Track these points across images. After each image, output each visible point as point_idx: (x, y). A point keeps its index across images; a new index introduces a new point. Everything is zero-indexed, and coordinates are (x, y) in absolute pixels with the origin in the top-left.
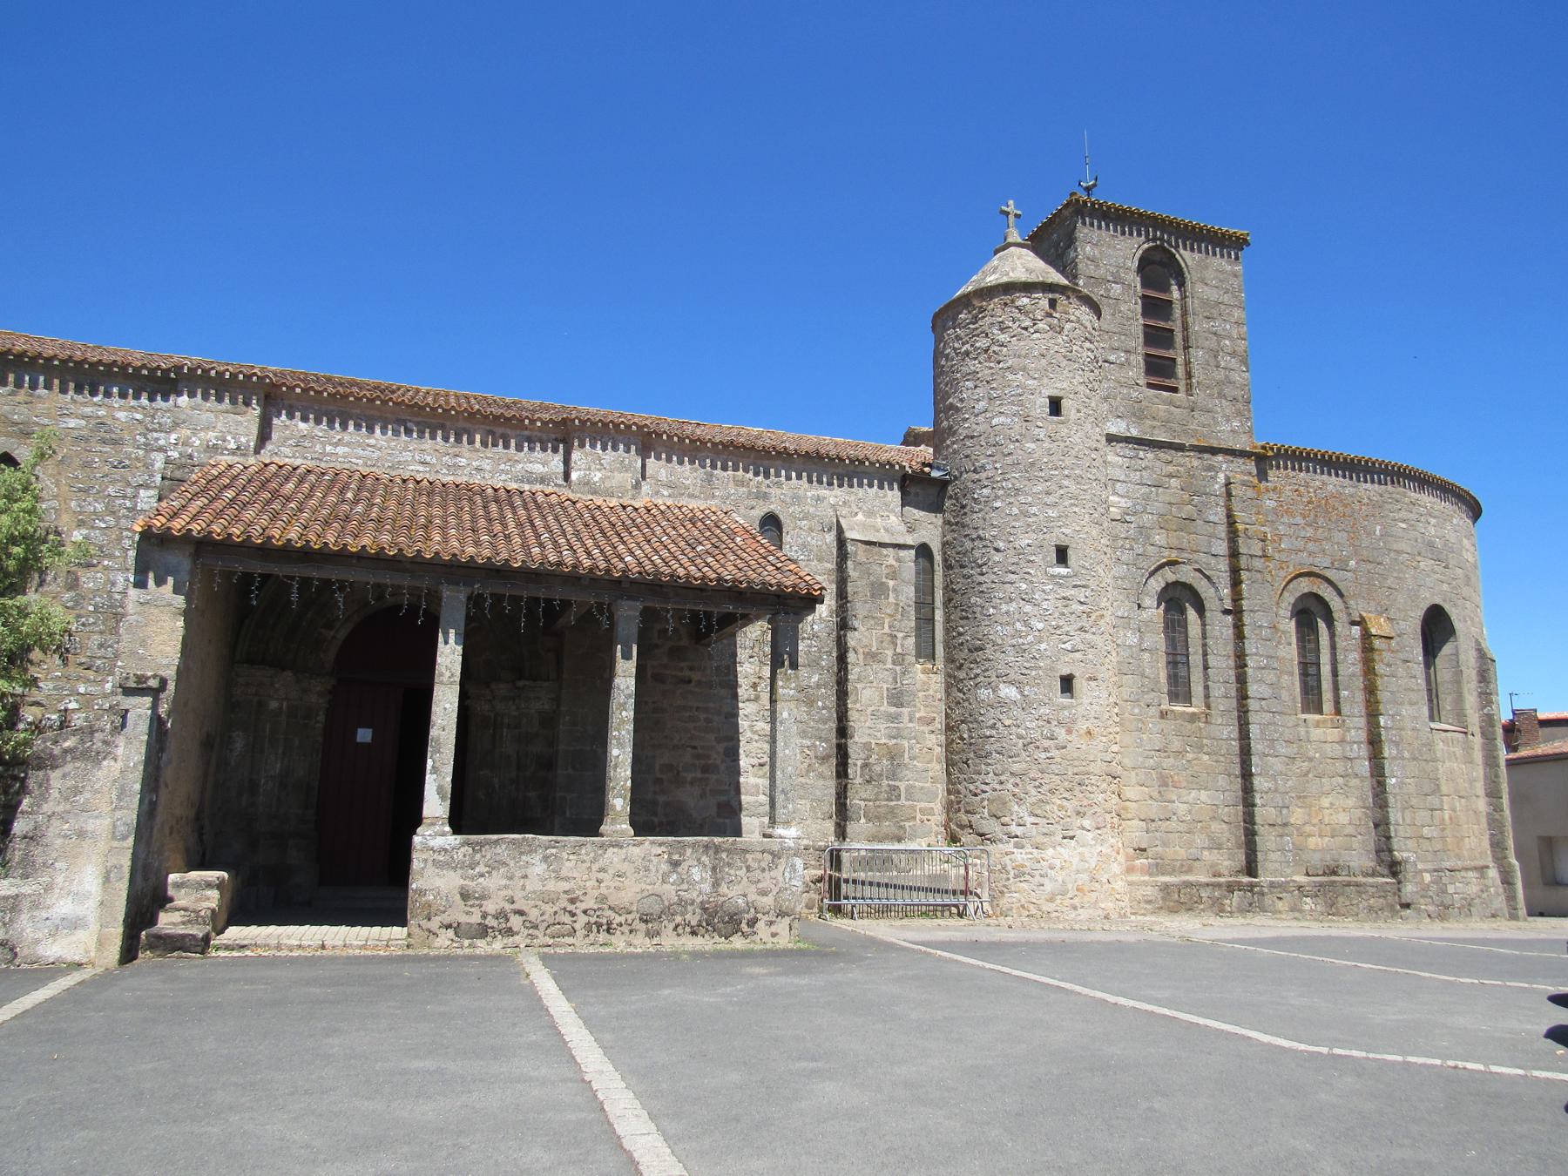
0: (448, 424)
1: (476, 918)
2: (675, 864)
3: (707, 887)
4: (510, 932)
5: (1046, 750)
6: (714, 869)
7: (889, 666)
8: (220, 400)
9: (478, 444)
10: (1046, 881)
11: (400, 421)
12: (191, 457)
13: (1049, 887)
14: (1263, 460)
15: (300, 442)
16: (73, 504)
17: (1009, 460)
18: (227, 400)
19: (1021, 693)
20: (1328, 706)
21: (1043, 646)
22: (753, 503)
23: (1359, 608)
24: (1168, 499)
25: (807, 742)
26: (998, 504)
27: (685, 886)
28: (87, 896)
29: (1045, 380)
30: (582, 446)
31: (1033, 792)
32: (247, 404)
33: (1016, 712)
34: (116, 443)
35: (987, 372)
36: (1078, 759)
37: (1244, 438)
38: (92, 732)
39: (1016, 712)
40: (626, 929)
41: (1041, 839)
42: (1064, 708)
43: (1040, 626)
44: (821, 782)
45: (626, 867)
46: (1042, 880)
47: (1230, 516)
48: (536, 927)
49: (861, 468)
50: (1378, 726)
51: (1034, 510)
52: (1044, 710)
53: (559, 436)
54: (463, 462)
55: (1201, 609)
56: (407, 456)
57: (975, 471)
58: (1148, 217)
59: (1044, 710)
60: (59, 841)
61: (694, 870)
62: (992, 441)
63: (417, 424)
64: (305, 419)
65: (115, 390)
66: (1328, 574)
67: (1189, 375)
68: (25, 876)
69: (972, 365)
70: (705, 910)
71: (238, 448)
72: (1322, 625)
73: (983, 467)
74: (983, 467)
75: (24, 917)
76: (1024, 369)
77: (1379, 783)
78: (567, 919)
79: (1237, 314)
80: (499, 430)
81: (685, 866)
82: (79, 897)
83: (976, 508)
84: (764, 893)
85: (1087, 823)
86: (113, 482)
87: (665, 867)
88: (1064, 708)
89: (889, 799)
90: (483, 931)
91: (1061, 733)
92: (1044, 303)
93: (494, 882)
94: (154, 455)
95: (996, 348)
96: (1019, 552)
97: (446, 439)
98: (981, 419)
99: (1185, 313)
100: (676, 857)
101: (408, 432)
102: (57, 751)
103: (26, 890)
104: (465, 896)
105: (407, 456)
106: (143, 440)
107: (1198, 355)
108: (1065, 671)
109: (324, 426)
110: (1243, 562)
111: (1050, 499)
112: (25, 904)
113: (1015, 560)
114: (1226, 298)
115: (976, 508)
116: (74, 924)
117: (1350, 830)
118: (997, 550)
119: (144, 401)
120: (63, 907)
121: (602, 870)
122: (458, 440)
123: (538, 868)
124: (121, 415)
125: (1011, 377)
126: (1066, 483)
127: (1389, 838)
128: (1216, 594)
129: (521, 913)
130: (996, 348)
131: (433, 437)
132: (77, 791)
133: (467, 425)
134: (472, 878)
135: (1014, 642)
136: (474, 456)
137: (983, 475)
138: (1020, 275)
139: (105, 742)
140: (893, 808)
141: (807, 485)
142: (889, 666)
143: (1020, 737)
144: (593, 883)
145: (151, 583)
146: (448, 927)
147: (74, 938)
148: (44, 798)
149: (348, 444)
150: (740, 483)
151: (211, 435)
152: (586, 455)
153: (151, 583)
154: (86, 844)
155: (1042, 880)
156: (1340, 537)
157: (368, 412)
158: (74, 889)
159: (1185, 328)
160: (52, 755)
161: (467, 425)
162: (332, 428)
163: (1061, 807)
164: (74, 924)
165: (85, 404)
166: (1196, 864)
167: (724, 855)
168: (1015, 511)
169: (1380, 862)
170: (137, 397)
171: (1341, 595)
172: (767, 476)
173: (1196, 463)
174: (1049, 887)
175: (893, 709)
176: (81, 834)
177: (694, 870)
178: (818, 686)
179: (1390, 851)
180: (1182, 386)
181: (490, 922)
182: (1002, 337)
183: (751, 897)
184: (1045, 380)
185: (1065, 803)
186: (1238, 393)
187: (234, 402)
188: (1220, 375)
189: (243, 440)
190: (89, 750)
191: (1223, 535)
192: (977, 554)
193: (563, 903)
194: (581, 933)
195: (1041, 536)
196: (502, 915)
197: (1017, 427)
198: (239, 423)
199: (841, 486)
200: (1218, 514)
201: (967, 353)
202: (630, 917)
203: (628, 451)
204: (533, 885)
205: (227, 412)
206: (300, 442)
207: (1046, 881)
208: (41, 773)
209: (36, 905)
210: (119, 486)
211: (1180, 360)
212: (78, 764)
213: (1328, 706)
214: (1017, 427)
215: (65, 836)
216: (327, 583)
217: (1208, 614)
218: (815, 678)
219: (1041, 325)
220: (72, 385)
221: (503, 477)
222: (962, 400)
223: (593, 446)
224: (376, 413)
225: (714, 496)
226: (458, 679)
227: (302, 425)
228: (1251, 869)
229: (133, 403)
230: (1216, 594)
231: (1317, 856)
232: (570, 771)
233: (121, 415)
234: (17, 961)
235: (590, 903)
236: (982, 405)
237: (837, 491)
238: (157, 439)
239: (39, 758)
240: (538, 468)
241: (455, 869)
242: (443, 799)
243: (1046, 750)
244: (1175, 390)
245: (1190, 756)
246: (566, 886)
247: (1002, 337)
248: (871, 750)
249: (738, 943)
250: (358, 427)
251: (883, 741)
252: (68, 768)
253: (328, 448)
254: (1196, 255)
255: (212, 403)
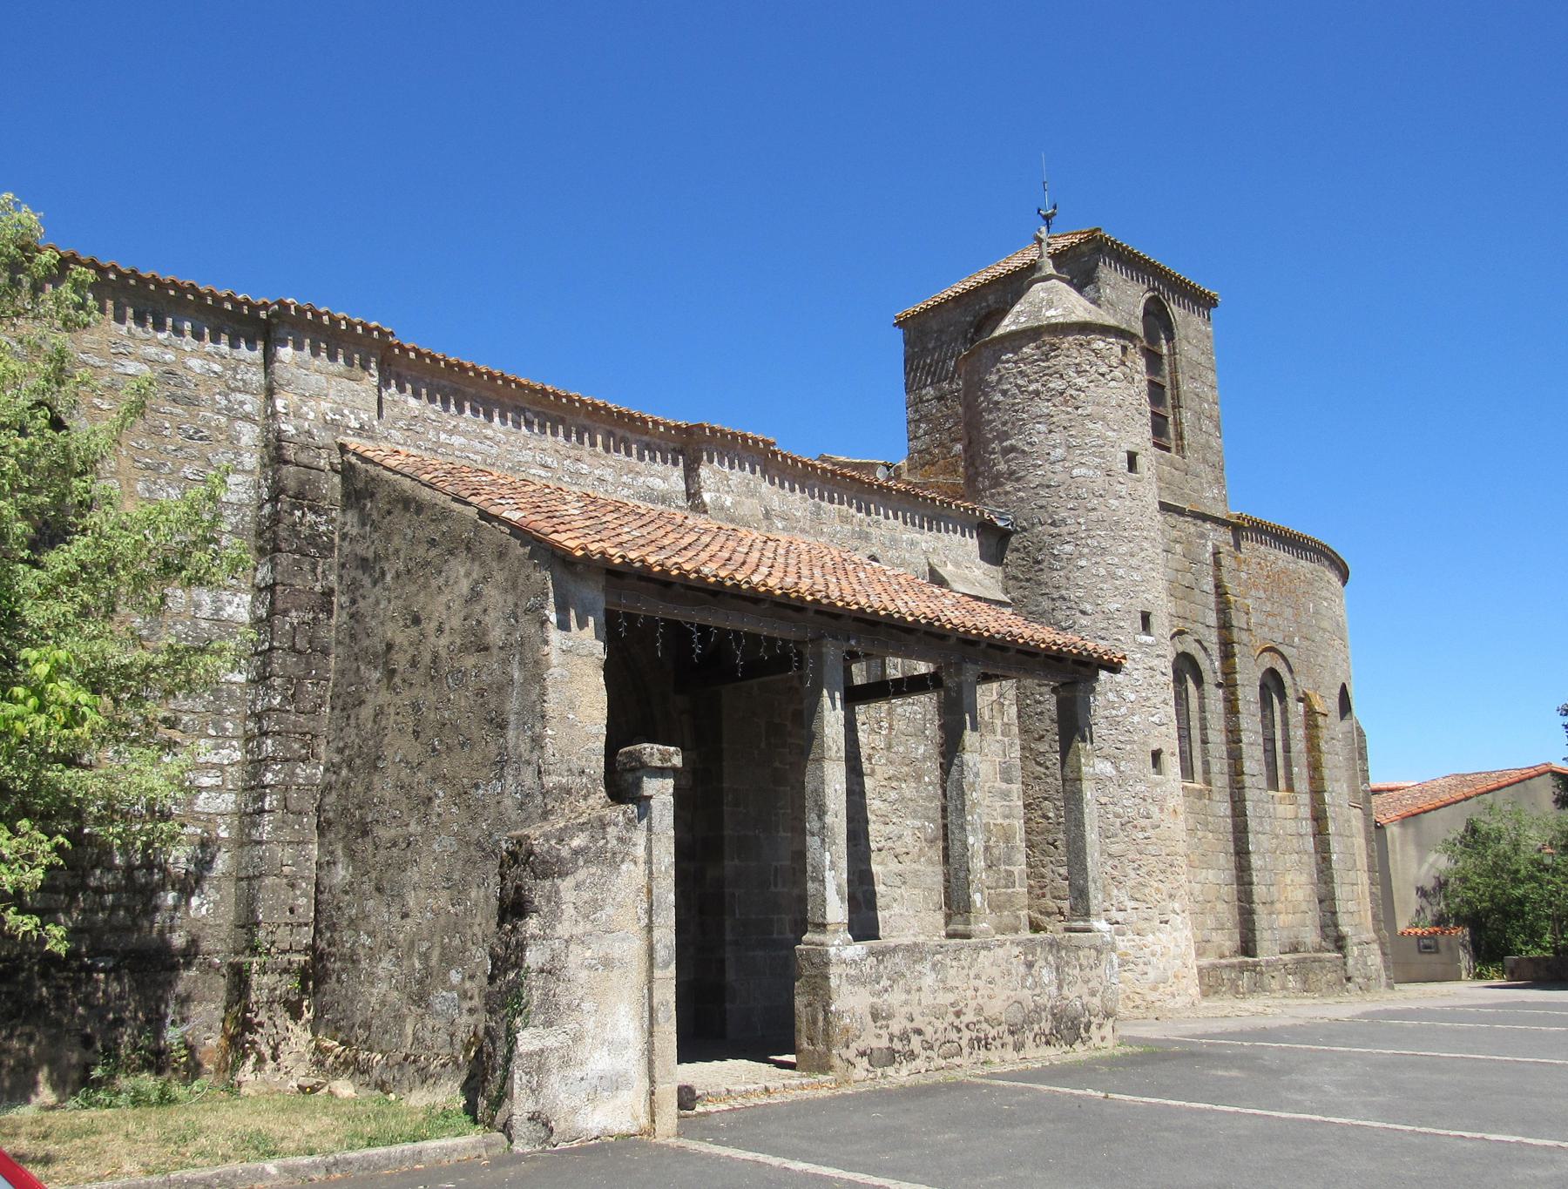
0: (568, 418)
1: (884, 1043)
2: (1030, 965)
3: (1053, 990)
4: (912, 1056)
5: (1143, 829)
6: (1057, 969)
7: (999, 737)
8: (333, 357)
9: (600, 448)
10: (1149, 969)
11: (519, 410)
12: (310, 434)
13: (1152, 975)
14: (1240, 529)
15: (412, 424)
16: (140, 486)
17: (1093, 516)
18: (341, 360)
19: (1117, 768)
20: (1282, 783)
21: (1136, 719)
22: (856, 543)
23: (1304, 685)
24: (1176, 565)
25: (918, 823)
26: (1083, 563)
27: (1038, 991)
28: (625, 1045)
29: (1123, 434)
30: (711, 461)
31: (1132, 874)
32: (365, 367)
33: (1112, 789)
34: (191, 402)
35: (1063, 416)
36: (1169, 839)
37: (1221, 506)
38: (604, 826)
39: (1112, 789)
40: (998, 1043)
41: (1142, 925)
42: (1157, 785)
43: (1133, 697)
44: (930, 869)
45: (995, 972)
46: (1146, 969)
47: (1219, 586)
48: (931, 1048)
49: (947, 512)
50: (1323, 802)
51: (1121, 572)
52: (1140, 787)
53: (678, 446)
54: (585, 468)
55: (1199, 681)
56: (527, 456)
57: (1053, 524)
58: (1152, 264)
59: (1140, 787)
60: (584, 974)
61: (1044, 971)
62: (1073, 493)
63: (537, 415)
64: (417, 395)
65: (187, 326)
66: (1281, 648)
67: (1180, 436)
68: (549, 1024)
69: (1044, 407)
70: (1054, 1015)
71: (362, 428)
72: (1276, 701)
73: (1064, 520)
74: (1064, 520)
75: (554, 1079)
76: (1103, 419)
77: (1324, 859)
78: (954, 1035)
79: (1211, 376)
80: (620, 432)
81: (1036, 967)
82: (615, 1047)
83: (1057, 565)
84: (1093, 994)
85: (1177, 906)
86: (190, 459)
87: (1022, 969)
88: (1157, 785)
89: (1007, 887)
90: (891, 1057)
91: (1154, 810)
92: (1117, 350)
93: (895, 998)
94: (239, 425)
95: (1074, 392)
96: (1108, 616)
97: (567, 437)
98: (1058, 467)
99: (1174, 371)
100: (1030, 958)
101: (529, 424)
102: (565, 852)
103: (551, 1042)
104: (875, 1016)
105: (527, 456)
106: (224, 402)
107: (1187, 416)
108: (1155, 747)
109: (438, 406)
110: (1236, 635)
111: (1134, 562)
112: (554, 1061)
113: (1104, 625)
114: (1202, 359)
115: (1057, 565)
116: (614, 1083)
117: (1304, 907)
118: (1083, 613)
119: (224, 347)
120: (599, 1062)
121: (977, 977)
122: (580, 440)
123: (929, 980)
124: (195, 363)
125: (1091, 426)
126: (1146, 545)
127: (1334, 913)
128: (1211, 666)
129: (919, 1032)
130: (1074, 392)
131: (555, 433)
132: (596, 905)
133: (587, 422)
134: (879, 994)
135: (1107, 713)
136: (595, 462)
137: (1064, 530)
138: (1054, 315)
139: (620, 840)
140: (1010, 896)
141: (902, 526)
142: (999, 737)
143: (1117, 816)
144: (970, 993)
145: (573, 624)
146: (863, 1054)
147: (618, 1102)
148: (555, 915)
149: (464, 434)
150: (845, 519)
151: (325, 406)
152: (715, 473)
153: (573, 624)
154: (615, 974)
155: (1146, 969)
156: (1288, 612)
157: (486, 394)
158: (608, 1036)
159: (1175, 385)
160: (559, 859)
161: (587, 422)
162: (446, 409)
163: (1157, 889)
164: (614, 1083)
165: (147, 342)
166: (1208, 946)
167: (1063, 953)
168: (1103, 572)
169: (1325, 937)
170: (215, 340)
171: (1291, 671)
172: (868, 513)
173: (1193, 529)
174: (1152, 975)
175: (1004, 786)
176: (607, 963)
177: (1044, 971)
178: (925, 759)
179: (1336, 926)
180: (1173, 445)
181: (897, 1045)
182: (1080, 381)
183: (1086, 999)
184: (1123, 434)
185: (1161, 885)
186: (1215, 459)
187: (349, 362)
188: (1203, 439)
189: (364, 416)
190: (603, 850)
191: (1213, 606)
192: (1059, 615)
193: (951, 1018)
194: (966, 1050)
195: (1129, 601)
196: (904, 1037)
197: (1100, 481)
198: (354, 393)
199: (930, 529)
200: (1208, 584)
201: (1037, 393)
202: (1001, 1029)
203: (753, 472)
204: (927, 999)
205: (340, 375)
206: (412, 424)
207: (1149, 969)
208: (548, 883)
209: (566, 1062)
210: (197, 465)
211: (1170, 419)
212: (593, 870)
213: (1282, 783)
214: (1100, 481)
215: (590, 967)
216: (723, 633)
217: (1206, 687)
218: (921, 750)
219: (1117, 373)
220: (130, 312)
221: (626, 492)
222: (1031, 444)
223: (721, 463)
224: (494, 396)
225: (822, 533)
226: (843, 754)
227: (412, 402)
228: (1247, 947)
229: (209, 346)
230: (1211, 666)
231: (1285, 933)
232: (736, 862)
233: (195, 363)
234: (553, 1140)
235: (969, 1017)
236: (1059, 452)
237: (927, 535)
238: (242, 403)
239: (544, 862)
240: (657, 483)
241: (864, 984)
242: (842, 899)
243: (1143, 829)
244: (1168, 449)
245: (1200, 834)
246: (951, 997)
247: (1080, 381)
248: (990, 831)
249: (1080, 1052)
250: (475, 412)
251: (999, 821)
252: (581, 874)
253: (443, 436)
254: (1182, 311)
255: (322, 361)
